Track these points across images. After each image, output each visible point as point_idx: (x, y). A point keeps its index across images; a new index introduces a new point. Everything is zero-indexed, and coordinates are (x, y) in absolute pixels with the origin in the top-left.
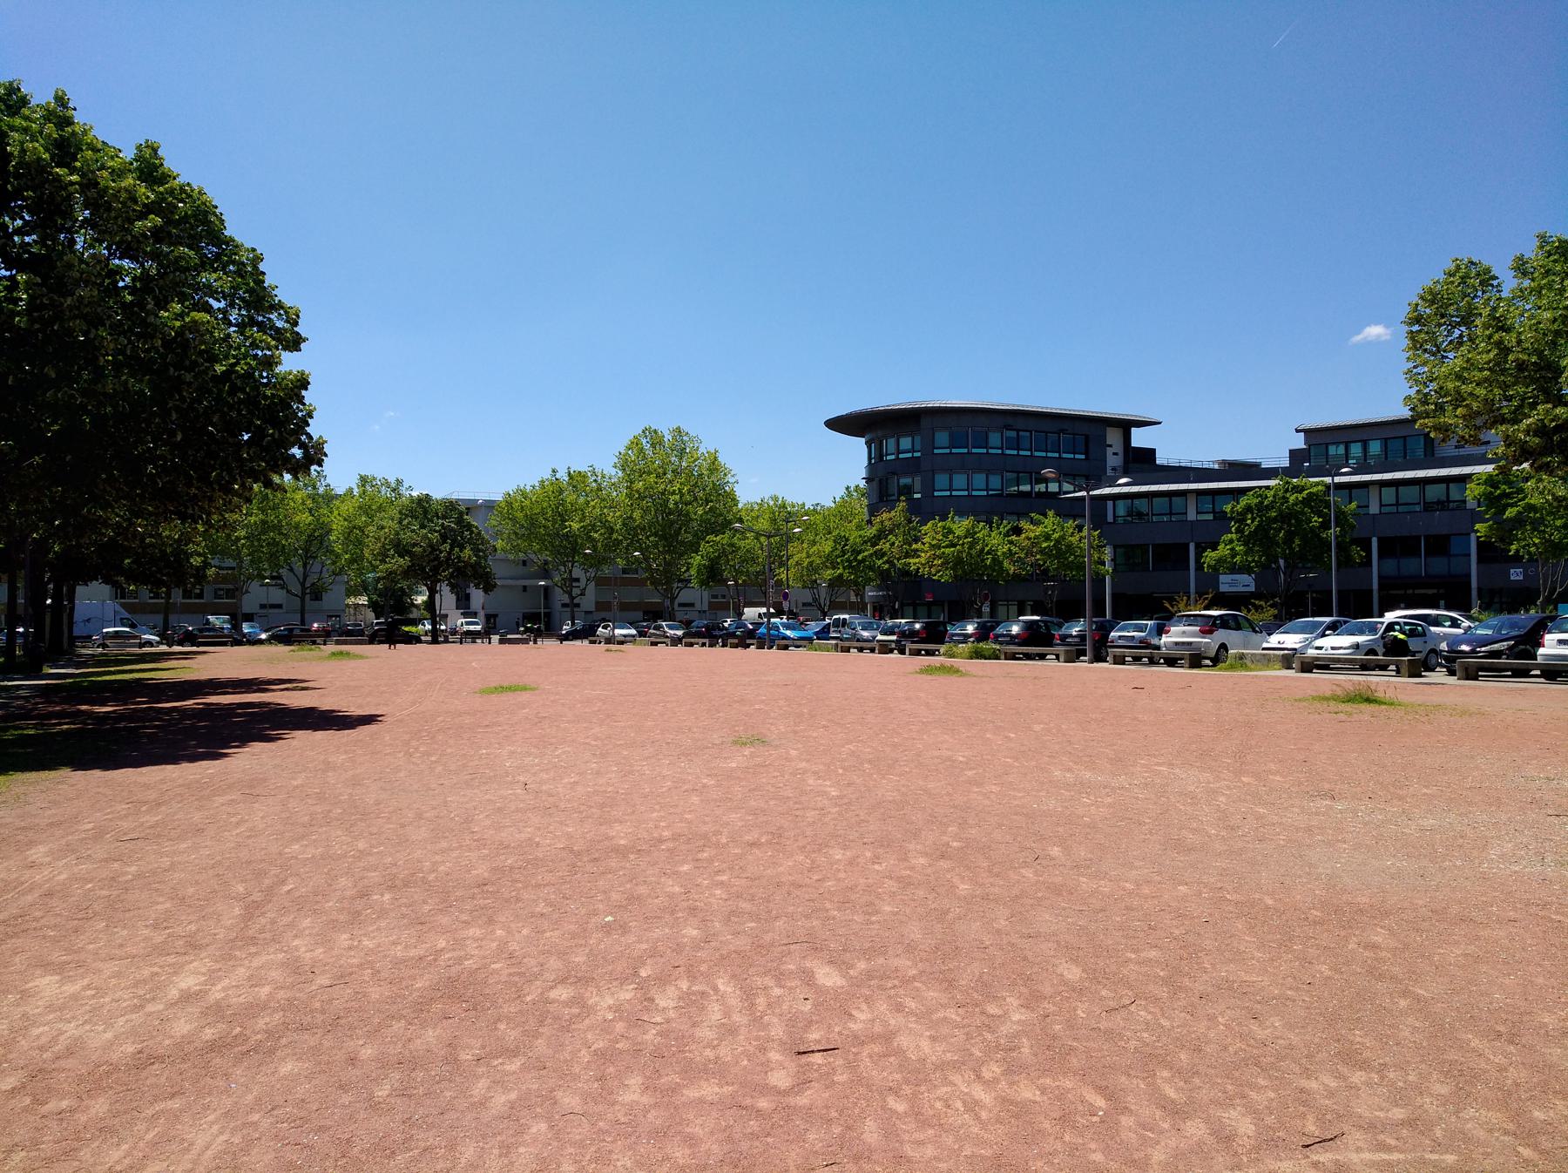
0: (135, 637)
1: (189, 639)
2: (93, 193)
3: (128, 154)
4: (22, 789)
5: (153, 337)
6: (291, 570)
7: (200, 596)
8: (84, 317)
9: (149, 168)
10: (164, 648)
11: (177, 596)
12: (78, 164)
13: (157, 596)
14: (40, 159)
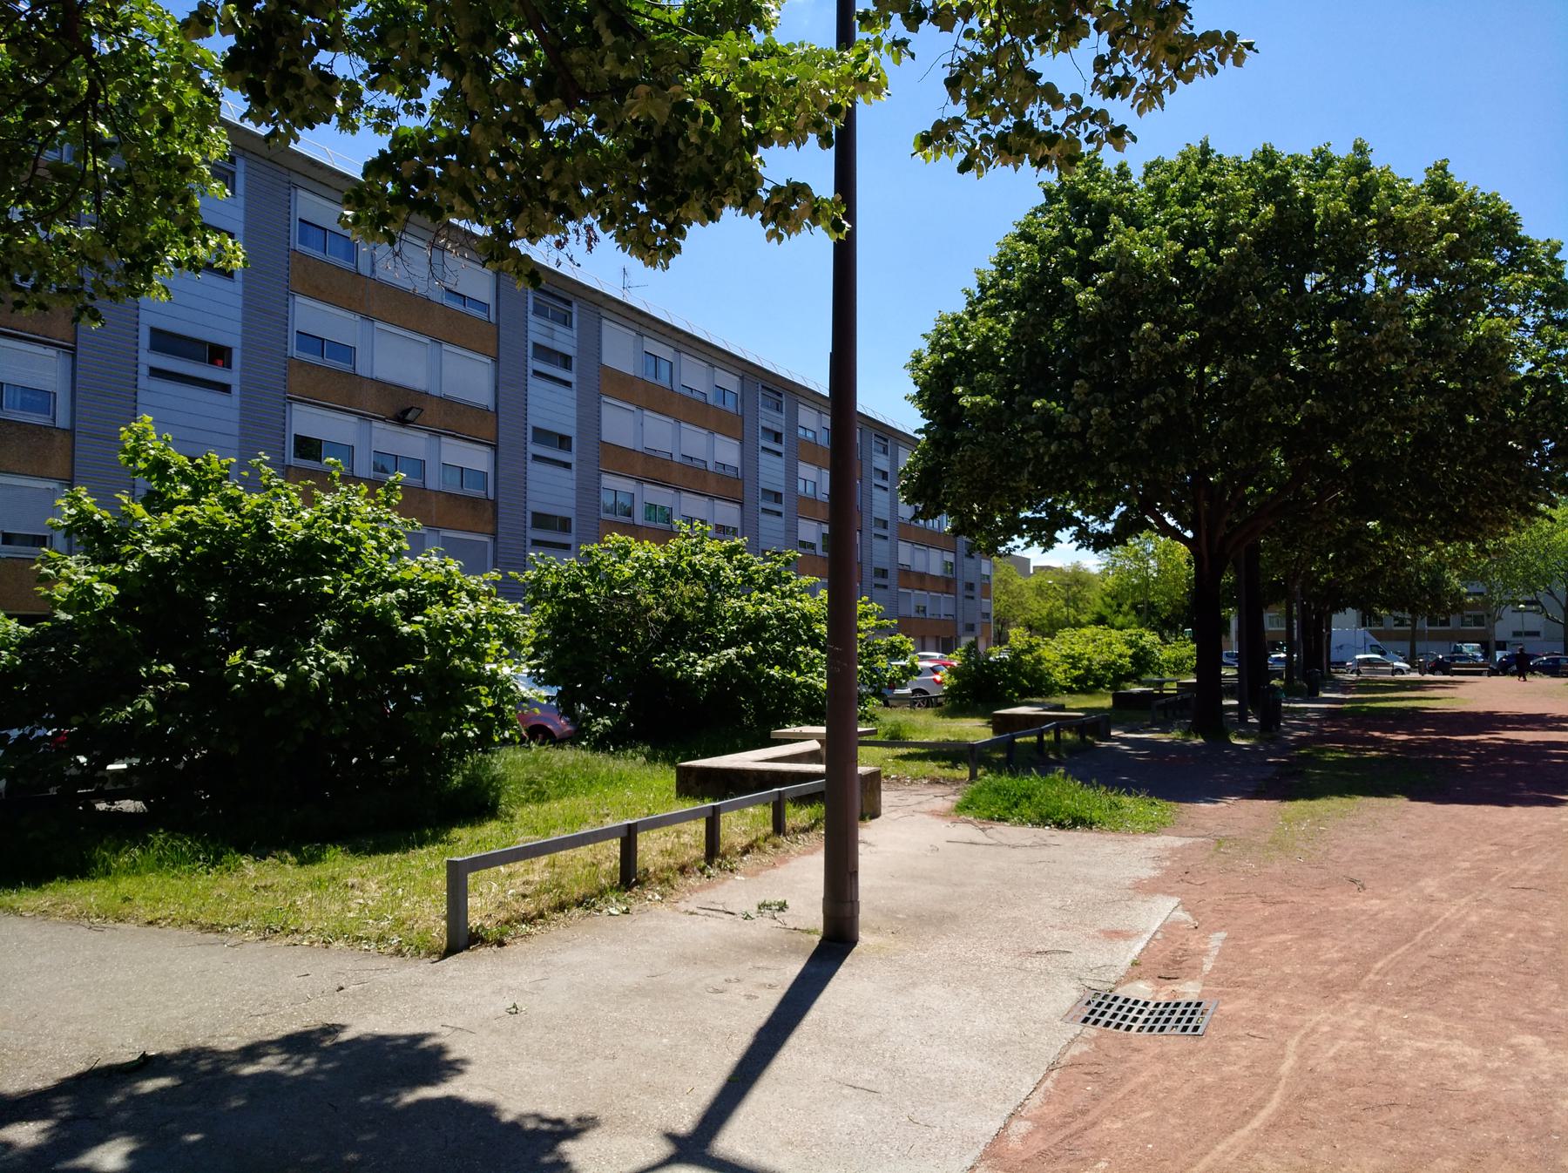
0: (1387, 664)
1: (1440, 667)
2: (1390, 232)
3: (1419, 180)
4: (1372, 814)
5: (1448, 354)
6: (1551, 593)
7: (1446, 623)
8: (1390, 349)
9: (1440, 190)
10: (1415, 676)
11: (1423, 624)
12: (1373, 207)
13: (1402, 623)
14: (1341, 213)
